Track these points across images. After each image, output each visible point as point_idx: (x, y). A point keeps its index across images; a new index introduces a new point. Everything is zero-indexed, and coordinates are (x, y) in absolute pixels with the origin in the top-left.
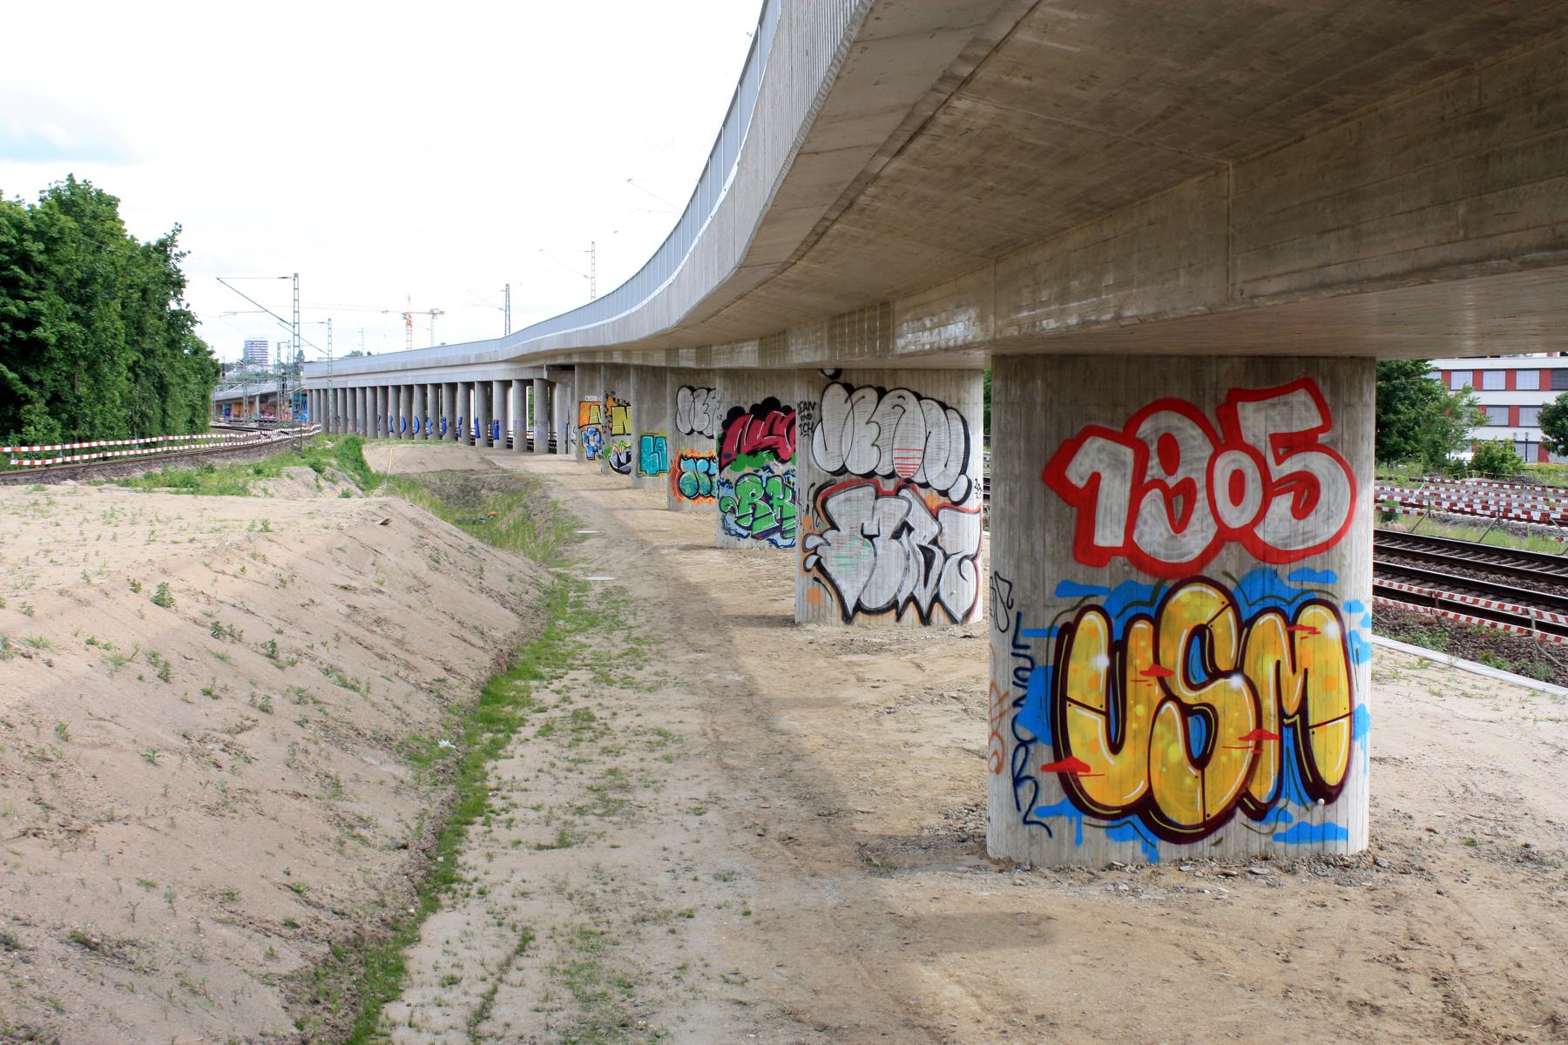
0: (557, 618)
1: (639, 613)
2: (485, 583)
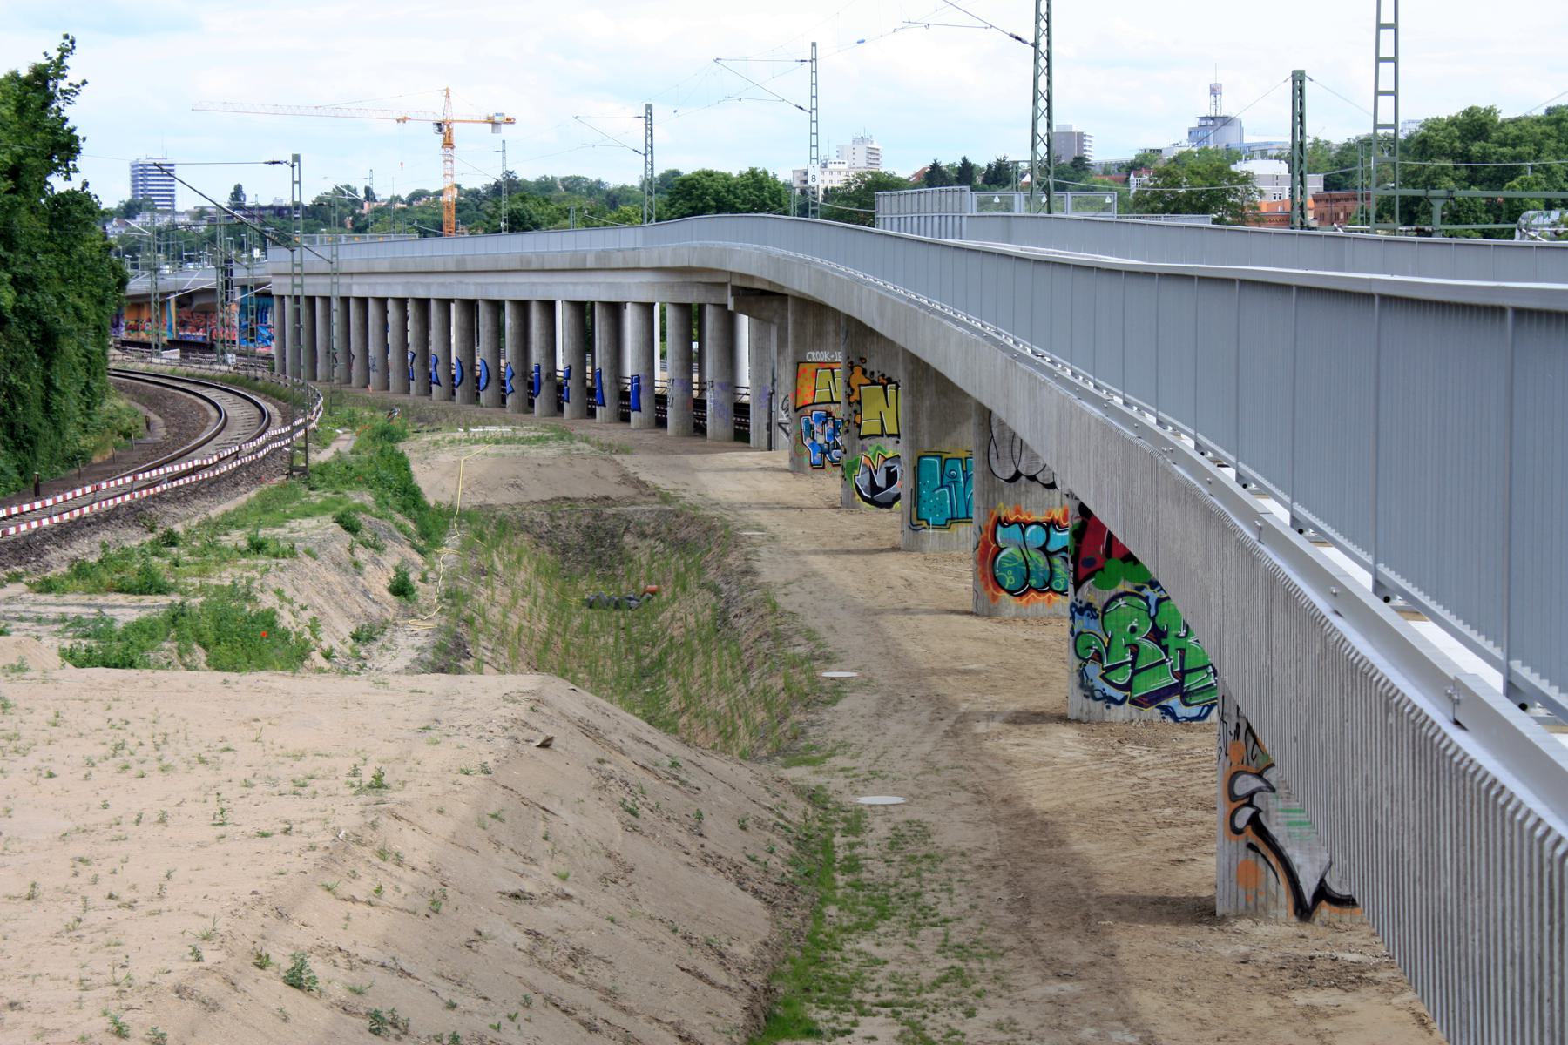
0: (824, 901)
1: (955, 886)
2: (710, 846)
